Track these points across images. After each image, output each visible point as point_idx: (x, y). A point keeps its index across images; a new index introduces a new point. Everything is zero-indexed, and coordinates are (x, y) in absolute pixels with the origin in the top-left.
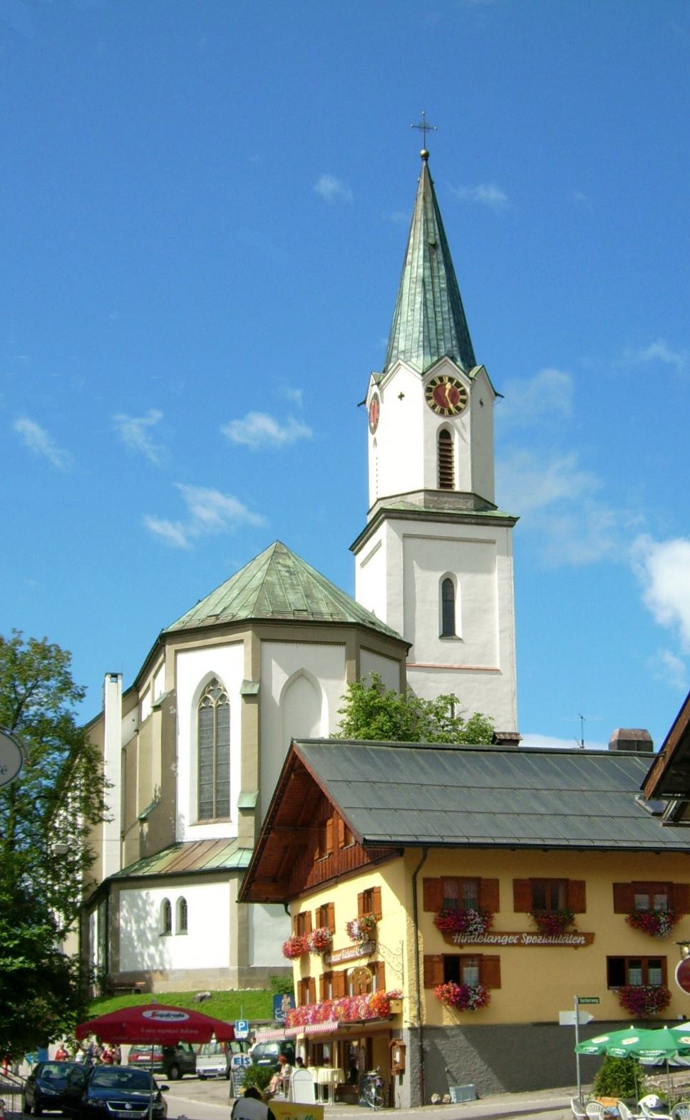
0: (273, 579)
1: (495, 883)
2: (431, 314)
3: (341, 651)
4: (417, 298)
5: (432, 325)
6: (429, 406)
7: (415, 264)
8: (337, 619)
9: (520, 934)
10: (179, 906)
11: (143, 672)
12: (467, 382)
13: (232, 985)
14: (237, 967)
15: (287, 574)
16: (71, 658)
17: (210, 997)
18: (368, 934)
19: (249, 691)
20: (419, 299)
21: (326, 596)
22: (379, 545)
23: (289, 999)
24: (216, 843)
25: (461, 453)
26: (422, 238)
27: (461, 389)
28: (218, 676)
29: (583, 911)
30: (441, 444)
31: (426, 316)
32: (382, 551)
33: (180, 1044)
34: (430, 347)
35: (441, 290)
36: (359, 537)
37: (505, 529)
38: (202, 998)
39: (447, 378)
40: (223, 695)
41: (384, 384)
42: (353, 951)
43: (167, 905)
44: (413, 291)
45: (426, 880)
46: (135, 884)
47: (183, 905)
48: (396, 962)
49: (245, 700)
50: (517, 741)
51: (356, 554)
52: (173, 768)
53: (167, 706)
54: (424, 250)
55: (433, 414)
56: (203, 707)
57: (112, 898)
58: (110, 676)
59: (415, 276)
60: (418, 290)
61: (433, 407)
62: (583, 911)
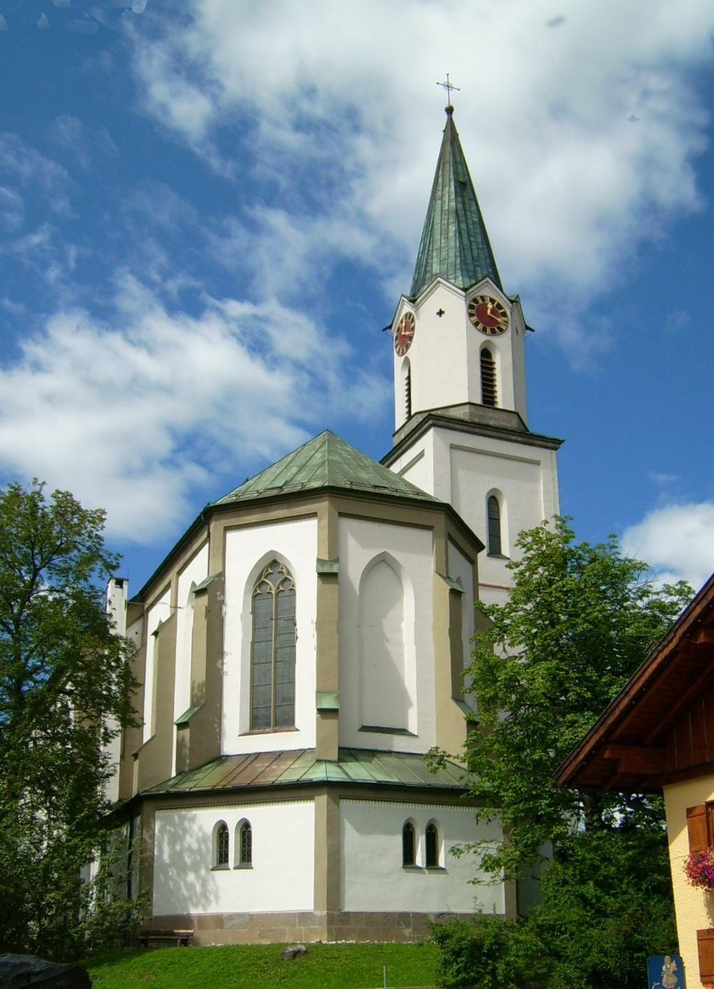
3: (427, 536)
4: (450, 227)
5: (468, 252)
6: (472, 322)
7: (446, 199)
10: (216, 834)
11: (160, 572)
12: (508, 305)
13: (319, 936)
14: (326, 911)
16: (105, 519)
17: (306, 952)
19: (326, 569)
20: (453, 228)
22: (421, 455)
23: (674, 964)
24: (279, 756)
25: (503, 372)
26: (452, 177)
28: (281, 556)
31: (461, 243)
32: (428, 459)
34: (468, 271)
37: (549, 451)
38: (296, 954)
39: (488, 299)
41: (420, 302)
43: (222, 829)
44: (446, 222)
46: (179, 803)
47: (245, 828)
49: (322, 580)
52: (219, 666)
53: (211, 592)
54: (455, 187)
55: (476, 330)
56: (259, 594)
58: (115, 581)
59: (447, 208)
60: (451, 221)
61: (476, 324)
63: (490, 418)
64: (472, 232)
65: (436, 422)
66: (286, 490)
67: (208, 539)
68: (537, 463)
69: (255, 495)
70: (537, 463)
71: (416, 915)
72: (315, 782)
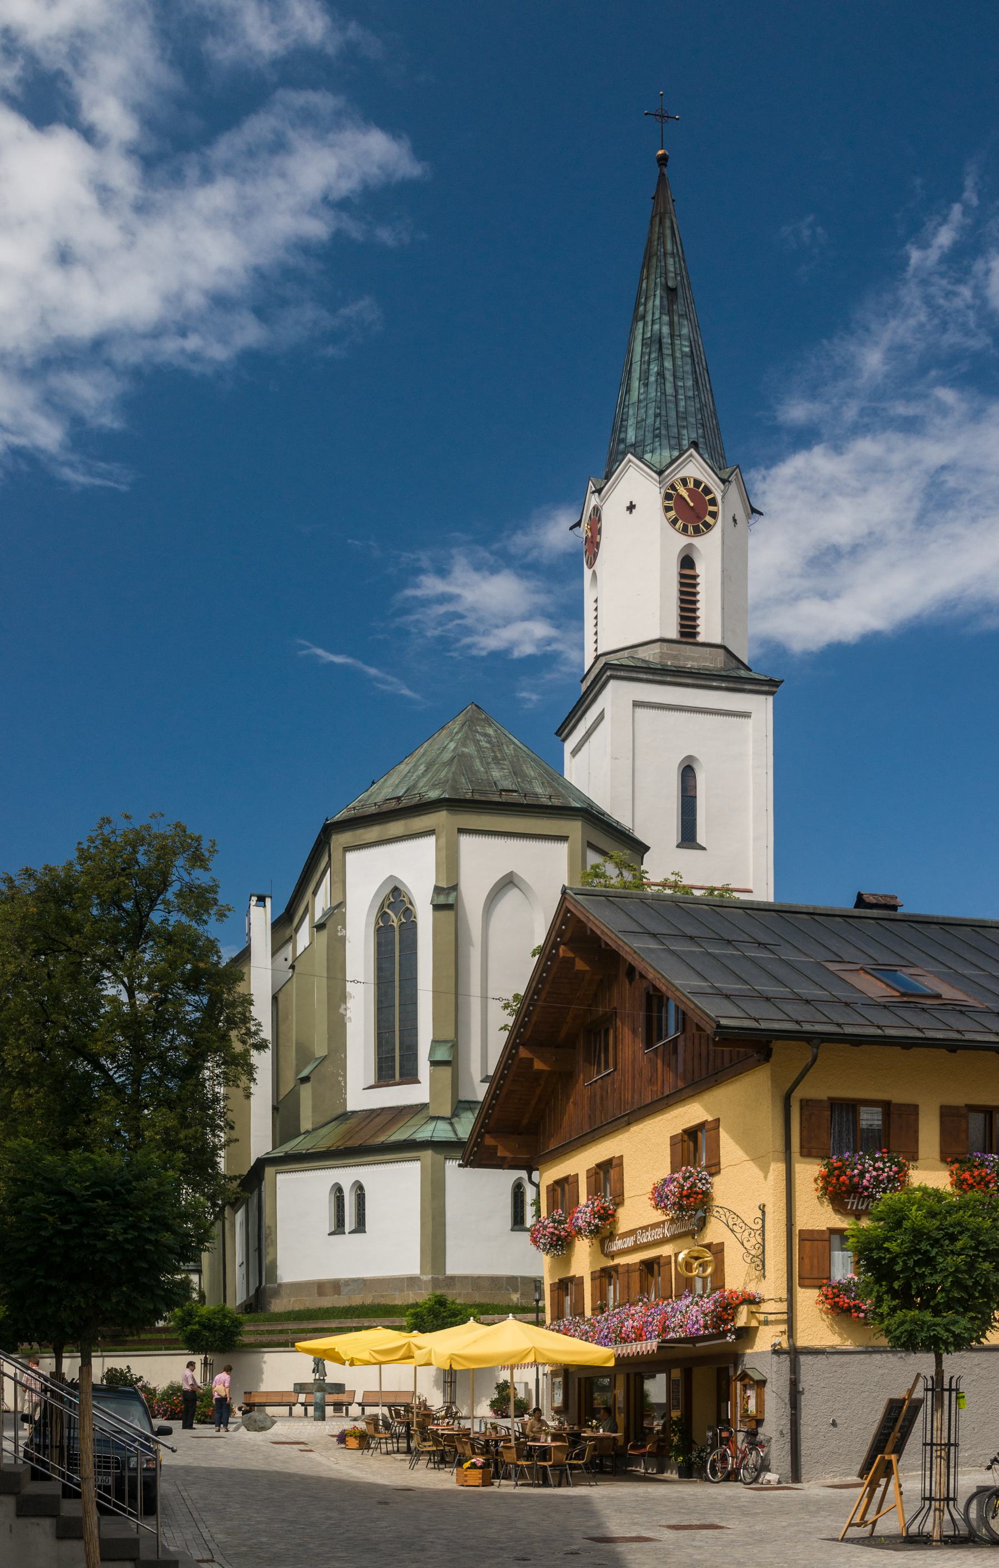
0: (470, 750)
1: (912, 1111)
2: (670, 390)
4: (651, 367)
6: (668, 519)
7: (649, 318)
8: (556, 802)
15: (488, 745)
18: (689, 1204)
19: (442, 900)
21: (540, 775)
22: (601, 717)
27: (711, 496)
30: (682, 576)
33: (884, 1283)
35: (684, 355)
36: (570, 713)
40: (408, 909)
42: (659, 1230)
43: (338, 1190)
44: (647, 358)
45: (805, 1104)
47: (359, 1190)
48: (753, 1241)
50: (894, 908)
51: (564, 740)
52: (342, 1011)
54: (661, 297)
57: (266, 1185)
61: (674, 522)
63: (688, 658)
64: (679, 374)
65: (615, 673)
66: (404, 803)
67: (329, 864)
68: (746, 715)
69: (373, 810)
70: (746, 715)
71: (524, 1279)
72: (420, 1142)
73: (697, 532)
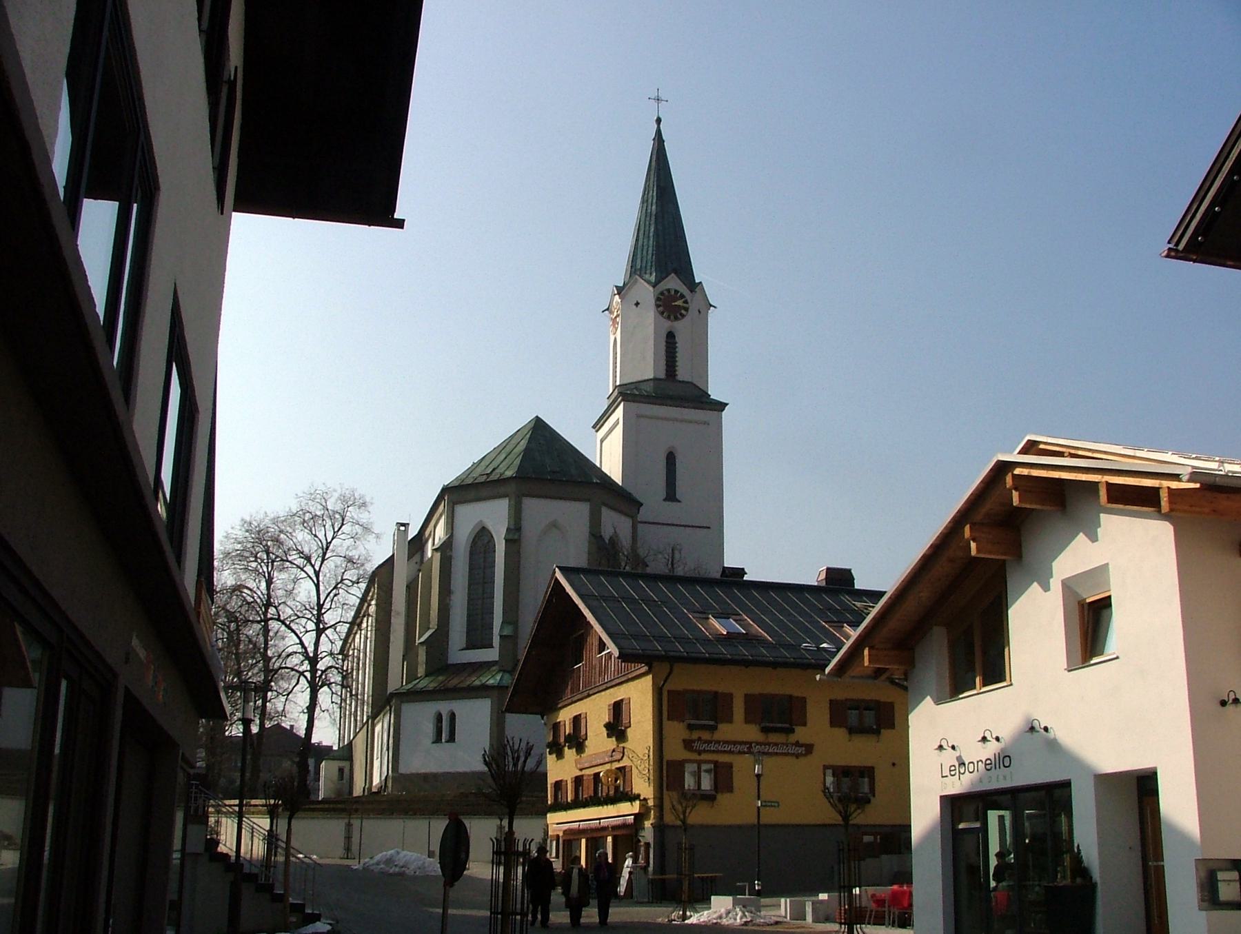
9: (750, 743)
19: (510, 537)
29: (804, 724)
43: (439, 718)
47: (453, 716)
61: (662, 313)
62: (804, 724)
73: (676, 319)
